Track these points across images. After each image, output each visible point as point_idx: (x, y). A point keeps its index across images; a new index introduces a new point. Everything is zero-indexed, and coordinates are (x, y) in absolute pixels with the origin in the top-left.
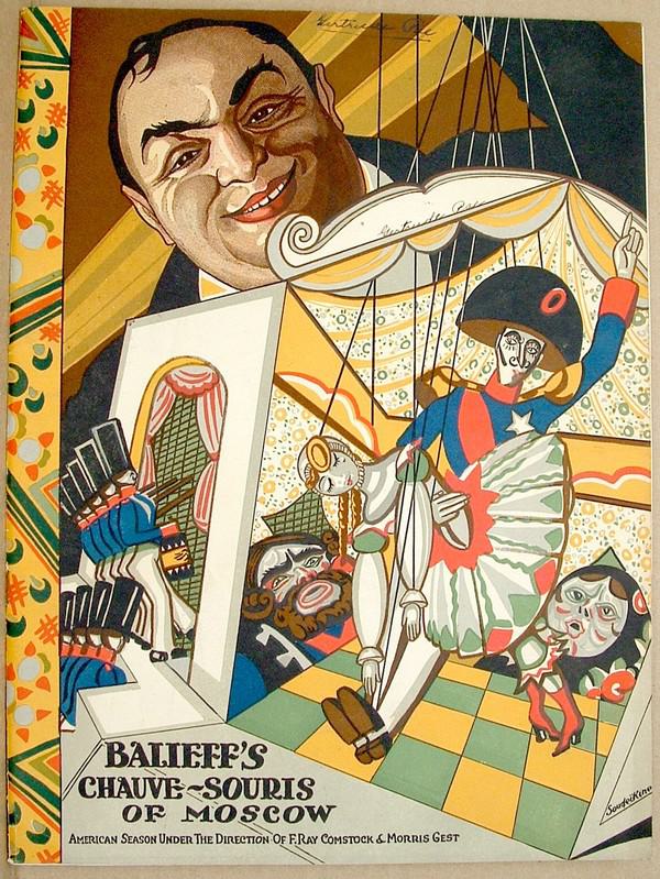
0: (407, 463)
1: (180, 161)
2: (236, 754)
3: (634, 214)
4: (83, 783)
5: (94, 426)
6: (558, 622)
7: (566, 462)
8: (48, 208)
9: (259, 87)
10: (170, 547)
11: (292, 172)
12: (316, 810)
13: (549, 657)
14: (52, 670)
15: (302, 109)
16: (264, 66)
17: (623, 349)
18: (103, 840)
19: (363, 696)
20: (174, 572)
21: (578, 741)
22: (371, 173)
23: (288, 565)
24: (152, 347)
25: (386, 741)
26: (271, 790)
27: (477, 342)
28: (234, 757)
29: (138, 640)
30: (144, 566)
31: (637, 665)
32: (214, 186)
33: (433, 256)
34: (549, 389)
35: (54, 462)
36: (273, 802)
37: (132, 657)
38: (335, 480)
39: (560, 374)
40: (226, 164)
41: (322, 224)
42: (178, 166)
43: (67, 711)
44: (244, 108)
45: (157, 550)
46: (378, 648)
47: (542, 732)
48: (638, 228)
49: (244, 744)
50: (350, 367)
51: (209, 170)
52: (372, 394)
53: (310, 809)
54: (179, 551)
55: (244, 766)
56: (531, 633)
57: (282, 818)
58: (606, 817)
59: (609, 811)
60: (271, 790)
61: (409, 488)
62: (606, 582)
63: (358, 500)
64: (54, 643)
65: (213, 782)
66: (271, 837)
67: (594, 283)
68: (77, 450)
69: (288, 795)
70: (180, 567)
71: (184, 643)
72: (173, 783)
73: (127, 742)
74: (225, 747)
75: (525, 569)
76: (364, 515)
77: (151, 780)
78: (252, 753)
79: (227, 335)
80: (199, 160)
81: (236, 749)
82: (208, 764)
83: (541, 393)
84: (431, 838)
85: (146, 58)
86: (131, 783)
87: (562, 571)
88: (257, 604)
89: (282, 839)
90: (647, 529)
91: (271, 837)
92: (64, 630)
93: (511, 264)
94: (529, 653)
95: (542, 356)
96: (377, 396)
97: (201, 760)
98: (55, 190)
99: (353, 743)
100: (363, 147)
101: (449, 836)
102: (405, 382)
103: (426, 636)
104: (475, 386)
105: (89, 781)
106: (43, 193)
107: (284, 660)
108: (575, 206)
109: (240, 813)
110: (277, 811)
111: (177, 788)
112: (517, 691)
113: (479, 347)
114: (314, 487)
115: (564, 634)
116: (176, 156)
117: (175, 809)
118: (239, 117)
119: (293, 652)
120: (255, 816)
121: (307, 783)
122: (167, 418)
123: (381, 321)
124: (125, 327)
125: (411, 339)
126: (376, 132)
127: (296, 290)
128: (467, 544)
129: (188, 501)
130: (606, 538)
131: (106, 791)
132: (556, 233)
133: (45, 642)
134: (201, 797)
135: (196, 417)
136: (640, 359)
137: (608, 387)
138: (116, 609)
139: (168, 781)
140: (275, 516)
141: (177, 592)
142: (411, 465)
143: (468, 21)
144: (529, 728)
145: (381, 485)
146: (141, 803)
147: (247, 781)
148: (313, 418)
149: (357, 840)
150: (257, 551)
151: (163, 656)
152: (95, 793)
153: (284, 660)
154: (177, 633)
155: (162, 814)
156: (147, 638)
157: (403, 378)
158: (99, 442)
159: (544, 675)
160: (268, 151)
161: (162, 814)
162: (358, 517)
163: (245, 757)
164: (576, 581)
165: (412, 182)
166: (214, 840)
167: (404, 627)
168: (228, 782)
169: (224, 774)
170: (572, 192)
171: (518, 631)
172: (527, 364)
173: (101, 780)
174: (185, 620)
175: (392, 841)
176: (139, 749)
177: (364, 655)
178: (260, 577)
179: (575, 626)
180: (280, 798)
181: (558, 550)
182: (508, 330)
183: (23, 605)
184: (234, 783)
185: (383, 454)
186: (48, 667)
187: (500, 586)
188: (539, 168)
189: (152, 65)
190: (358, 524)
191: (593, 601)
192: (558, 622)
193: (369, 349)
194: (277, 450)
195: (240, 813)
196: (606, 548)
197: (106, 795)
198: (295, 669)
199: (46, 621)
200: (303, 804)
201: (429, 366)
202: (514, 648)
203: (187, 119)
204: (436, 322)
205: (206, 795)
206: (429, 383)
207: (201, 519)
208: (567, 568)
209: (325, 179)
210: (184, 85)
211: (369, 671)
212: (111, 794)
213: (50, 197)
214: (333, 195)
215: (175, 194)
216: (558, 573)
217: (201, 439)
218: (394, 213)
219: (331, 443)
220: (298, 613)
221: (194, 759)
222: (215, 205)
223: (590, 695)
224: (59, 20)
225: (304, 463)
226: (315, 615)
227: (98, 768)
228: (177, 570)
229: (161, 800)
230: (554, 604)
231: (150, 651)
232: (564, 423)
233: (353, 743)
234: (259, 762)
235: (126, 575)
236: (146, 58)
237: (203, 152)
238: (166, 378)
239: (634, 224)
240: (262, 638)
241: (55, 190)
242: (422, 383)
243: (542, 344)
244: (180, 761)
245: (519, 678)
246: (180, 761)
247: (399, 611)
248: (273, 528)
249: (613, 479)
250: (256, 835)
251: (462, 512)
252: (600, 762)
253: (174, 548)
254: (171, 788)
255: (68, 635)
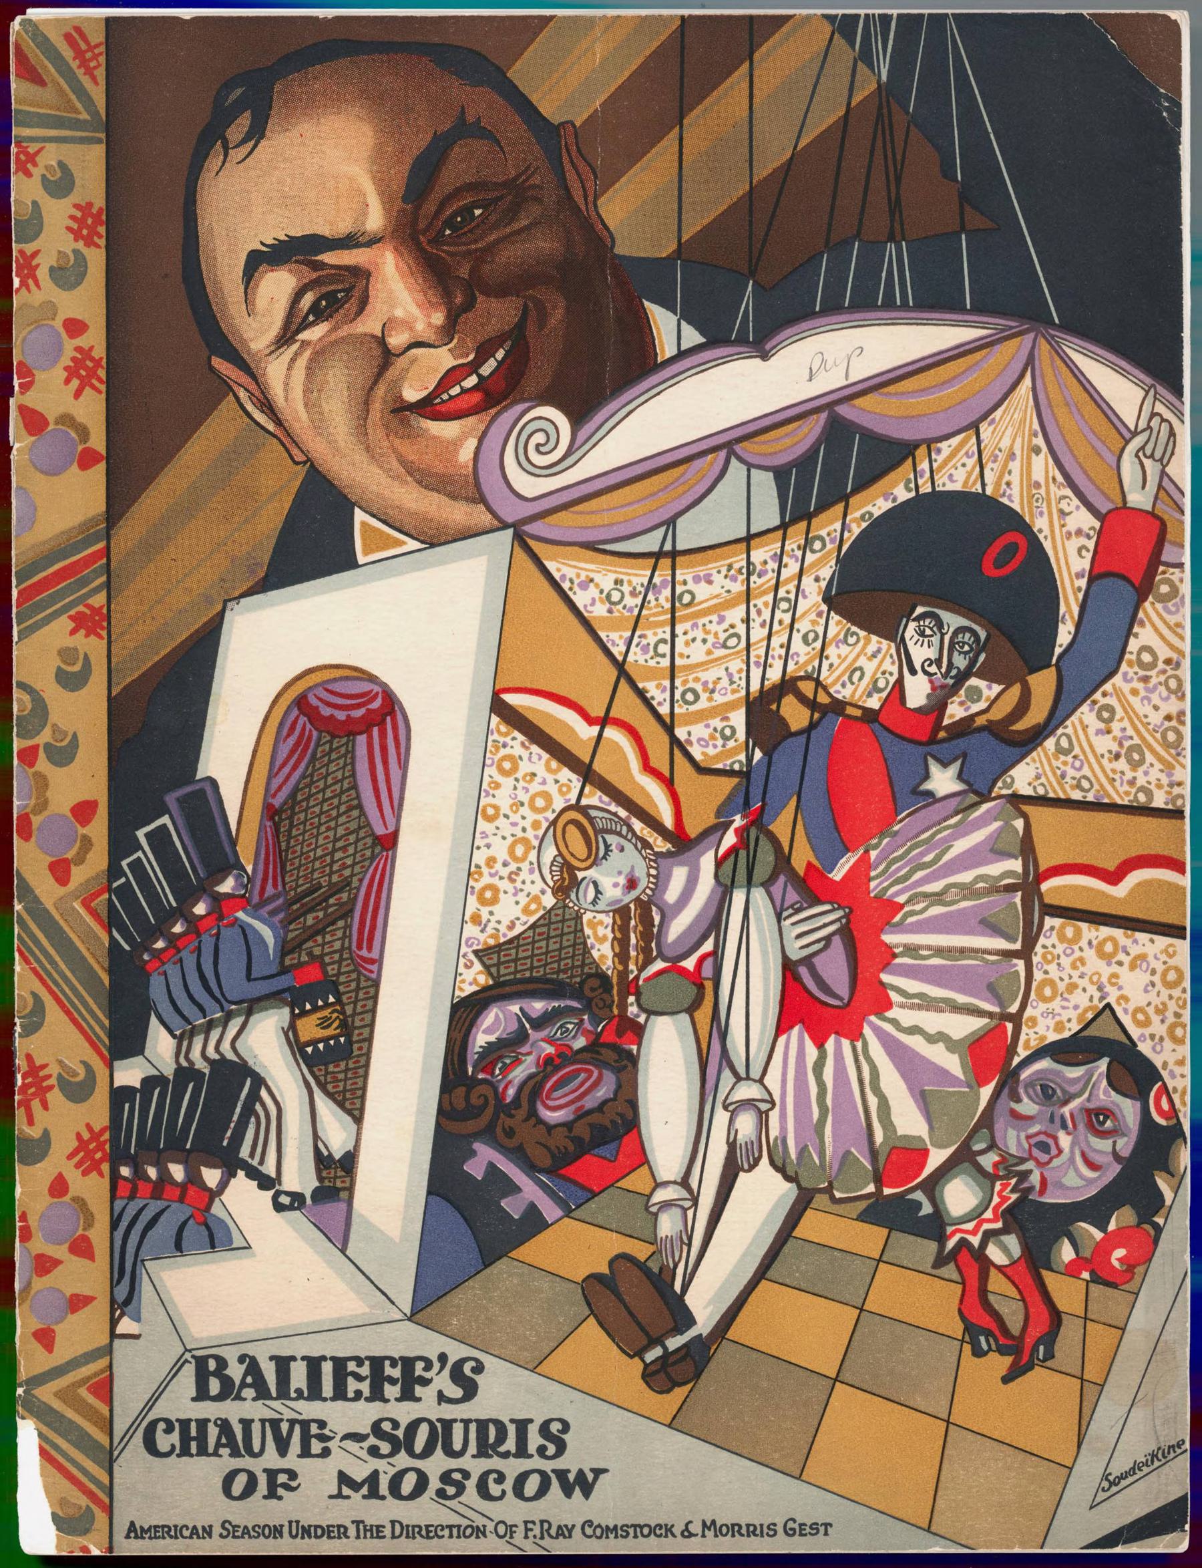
0: (733, 850)
1: (314, 308)
2: (427, 1375)
3: (1160, 388)
4: (153, 1425)
5: (169, 790)
6: (1013, 1140)
7: (1027, 848)
8: (78, 394)
9: (460, 167)
10: (308, 1007)
11: (521, 326)
12: (571, 1477)
13: (996, 1200)
14: (97, 1225)
15: (536, 210)
16: (464, 129)
17: (1133, 645)
18: (186, 1533)
19: (656, 1270)
20: (316, 1049)
21: (1050, 1355)
22: (668, 329)
23: (520, 1037)
24: (270, 646)
25: (698, 1356)
26: (492, 1440)
27: (862, 633)
28: (425, 1382)
29: (254, 1174)
30: (264, 1042)
31: (1160, 1220)
32: (377, 352)
33: (781, 475)
34: (997, 714)
35: (98, 860)
36: (495, 1463)
37: (242, 1201)
38: (606, 883)
39: (1016, 690)
40: (399, 313)
41: (578, 418)
42: (311, 318)
43: (124, 1302)
44: (430, 207)
45: (286, 1011)
46: (684, 1183)
47: (982, 1339)
48: (1167, 415)
49: (443, 1358)
50: (632, 683)
51: (370, 324)
52: (669, 729)
53: (562, 1475)
54: (326, 1013)
55: (442, 1398)
56: (963, 1158)
57: (510, 1493)
58: (1102, 1496)
59: (1106, 1484)
60: (492, 1440)
61: (739, 897)
62: (1103, 1065)
63: (646, 920)
64: (101, 1174)
65: (387, 1426)
66: (490, 1526)
67: (1084, 520)
68: (141, 834)
69: (522, 1451)
70: (325, 1040)
71: (336, 1175)
72: (314, 1429)
73: (231, 1355)
74: (408, 1363)
75: (952, 1045)
76: (658, 945)
77: (275, 1424)
78: (457, 1375)
79: (412, 622)
80: (352, 306)
81: (428, 1368)
82: (377, 1395)
83: (980, 721)
84: (780, 1529)
85: (244, 122)
86: (238, 1430)
87: (1020, 1049)
88: (467, 1100)
89: (511, 1529)
90: (1178, 970)
91: (490, 1526)
92: (118, 1156)
93: (926, 489)
94: (960, 1196)
95: (982, 657)
96: (681, 733)
97: (365, 1387)
98: (90, 364)
99: (640, 1354)
100: (653, 279)
101: (815, 1527)
102: (731, 706)
103: (772, 1163)
104: (858, 713)
105: (162, 1426)
106: (66, 368)
107: (512, 1207)
108: (1048, 371)
109: (434, 1484)
110: (501, 1478)
111: (323, 1438)
112: (940, 1261)
113: (868, 642)
114: (568, 897)
115: (1023, 1161)
116: (308, 299)
117: (318, 1477)
118: (422, 225)
119: (530, 1191)
120: (461, 1489)
121: (555, 1427)
122: (303, 777)
123: (687, 598)
124: (221, 615)
125: (741, 629)
126: (674, 246)
127: (531, 543)
128: (844, 992)
129: (341, 923)
130: (1100, 989)
131: (194, 1444)
132: (1011, 427)
133: (84, 1173)
134: (364, 1454)
135: (353, 775)
136: (1168, 662)
137: (1106, 715)
138: (212, 1118)
139: (305, 1424)
140: (499, 948)
141: (323, 1087)
142: (743, 853)
143: (845, 26)
144: (957, 1329)
145: (691, 888)
146: (256, 1466)
147: (448, 1424)
148: (566, 774)
149: (646, 1531)
150: (465, 1013)
151: (297, 1200)
152: (173, 1446)
153: (512, 1207)
154: (322, 1161)
155: (294, 1484)
156: (270, 1169)
157: (730, 697)
158: (180, 822)
159: (988, 1235)
160: (476, 287)
161: (294, 1484)
162: (646, 950)
163: (442, 1381)
164: (1045, 1064)
165: (742, 340)
166: (387, 1532)
167: (732, 1145)
168: (413, 1426)
169: (405, 1413)
170: (1044, 346)
171: (937, 1158)
172: (954, 672)
173: (185, 1424)
174: (337, 1137)
175: (710, 1534)
176: (253, 1367)
177: (660, 1196)
178: (472, 1057)
179: (1044, 1147)
180: (506, 1455)
181: (1014, 1009)
182: (920, 610)
183: (45, 1106)
184: (424, 1430)
185: (693, 835)
186: (90, 1222)
187: (902, 1070)
188: (977, 309)
189: (257, 133)
190: (648, 961)
191: (1075, 1104)
192: (1013, 1140)
193: (665, 649)
194: (500, 833)
195: (434, 1484)
196: (1101, 1006)
197: (194, 1450)
198: (534, 1223)
199: (86, 1136)
200: (548, 1466)
201: (774, 675)
202: (932, 1185)
203: (325, 230)
204: (788, 600)
205: (374, 1451)
206: (774, 707)
207: (364, 953)
208: (1031, 1037)
209: (572, 338)
210: (318, 171)
211: (668, 1225)
212: (203, 1451)
213: (79, 377)
214: (601, 370)
215: (308, 368)
216: (1012, 1050)
217: (363, 813)
218: (708, 398)
219: (580, 835)
220: (541, 1121)
221: (352, 1385)
222: (381, 390)
223: (1072, 1270)
224: (83, 46)
225: (550, 852)
226: (568, 1125)
227: (181, 1402)
228: (321, 1046)
229: (292, 1460)
230: (1004, 1102)
231: (272, 1192)
232: (1023, 777)
233: (640, 1354)
234: (470, 1390)
235: (230, 1056)
236: (244, 122)
237: (357, 293)
238: (301, 702)
239: (1159, 408)
240: (475, 1168)
241: (90, 364)
242: (762, 710)
243: (983, 635)
244: (328, 1388)
245: (942, 1239)
246: (328, 1388)
247: (722, 1117)
248: (494, 970)
249: (1114, 877)
250: (465, 1522)
251: (837, 940)
252: (1089, 1390)
253: (316, 1009)
254: (313, 1437)
255: (125, 1165)
